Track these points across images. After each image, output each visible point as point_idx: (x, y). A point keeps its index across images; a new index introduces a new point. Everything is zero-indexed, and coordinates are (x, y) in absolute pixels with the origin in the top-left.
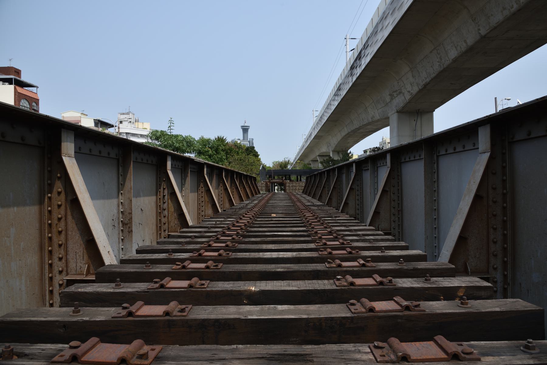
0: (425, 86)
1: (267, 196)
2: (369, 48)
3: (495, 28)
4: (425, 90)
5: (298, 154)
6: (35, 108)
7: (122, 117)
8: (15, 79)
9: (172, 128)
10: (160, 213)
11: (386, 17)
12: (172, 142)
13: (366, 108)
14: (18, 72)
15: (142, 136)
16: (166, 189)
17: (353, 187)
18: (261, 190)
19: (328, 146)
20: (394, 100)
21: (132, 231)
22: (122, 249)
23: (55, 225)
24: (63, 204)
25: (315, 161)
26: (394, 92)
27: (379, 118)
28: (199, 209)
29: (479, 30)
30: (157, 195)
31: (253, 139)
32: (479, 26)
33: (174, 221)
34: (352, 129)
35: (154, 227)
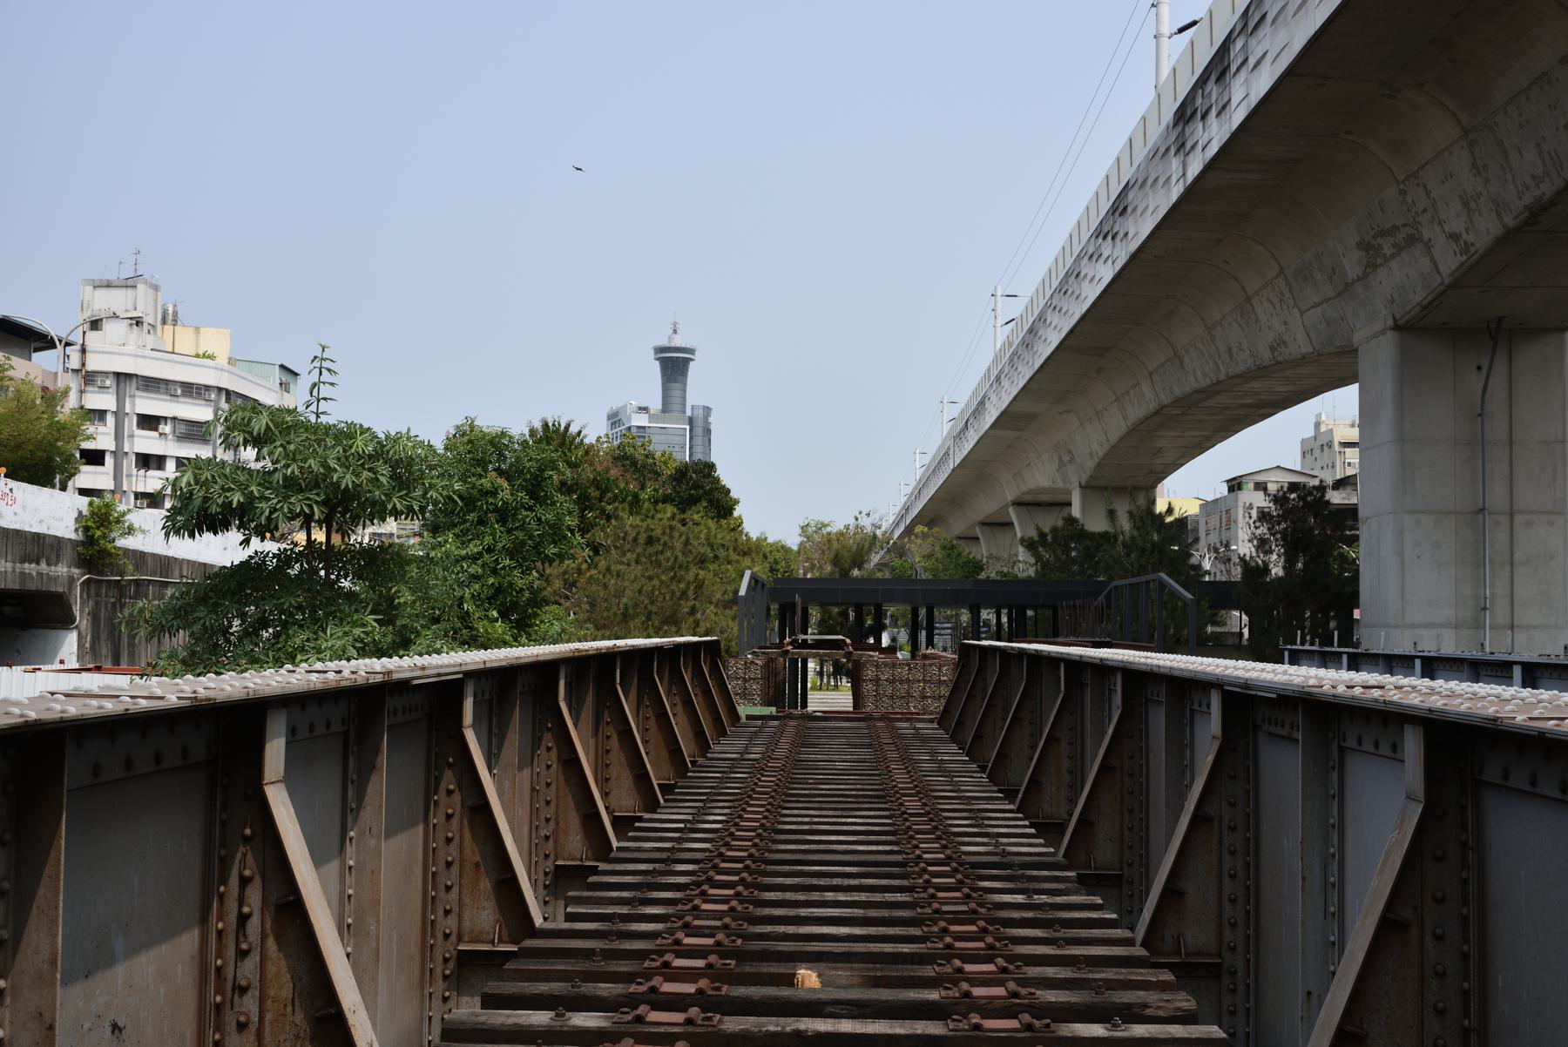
0: (1536, 214)
2: (1266, 29)
5: (919, 492)
9: (325, 391)
10: (218, 1007)
13: (1248, 300)
15: (192, 390)
16: (257, 881)
18: (746, 696)
19: (1062, 464)
20: (1382, 272)
26: (1382, 233)
27: (1306, 348)
28: (428, 903)
30: (204, 919)
31: (707, 410)
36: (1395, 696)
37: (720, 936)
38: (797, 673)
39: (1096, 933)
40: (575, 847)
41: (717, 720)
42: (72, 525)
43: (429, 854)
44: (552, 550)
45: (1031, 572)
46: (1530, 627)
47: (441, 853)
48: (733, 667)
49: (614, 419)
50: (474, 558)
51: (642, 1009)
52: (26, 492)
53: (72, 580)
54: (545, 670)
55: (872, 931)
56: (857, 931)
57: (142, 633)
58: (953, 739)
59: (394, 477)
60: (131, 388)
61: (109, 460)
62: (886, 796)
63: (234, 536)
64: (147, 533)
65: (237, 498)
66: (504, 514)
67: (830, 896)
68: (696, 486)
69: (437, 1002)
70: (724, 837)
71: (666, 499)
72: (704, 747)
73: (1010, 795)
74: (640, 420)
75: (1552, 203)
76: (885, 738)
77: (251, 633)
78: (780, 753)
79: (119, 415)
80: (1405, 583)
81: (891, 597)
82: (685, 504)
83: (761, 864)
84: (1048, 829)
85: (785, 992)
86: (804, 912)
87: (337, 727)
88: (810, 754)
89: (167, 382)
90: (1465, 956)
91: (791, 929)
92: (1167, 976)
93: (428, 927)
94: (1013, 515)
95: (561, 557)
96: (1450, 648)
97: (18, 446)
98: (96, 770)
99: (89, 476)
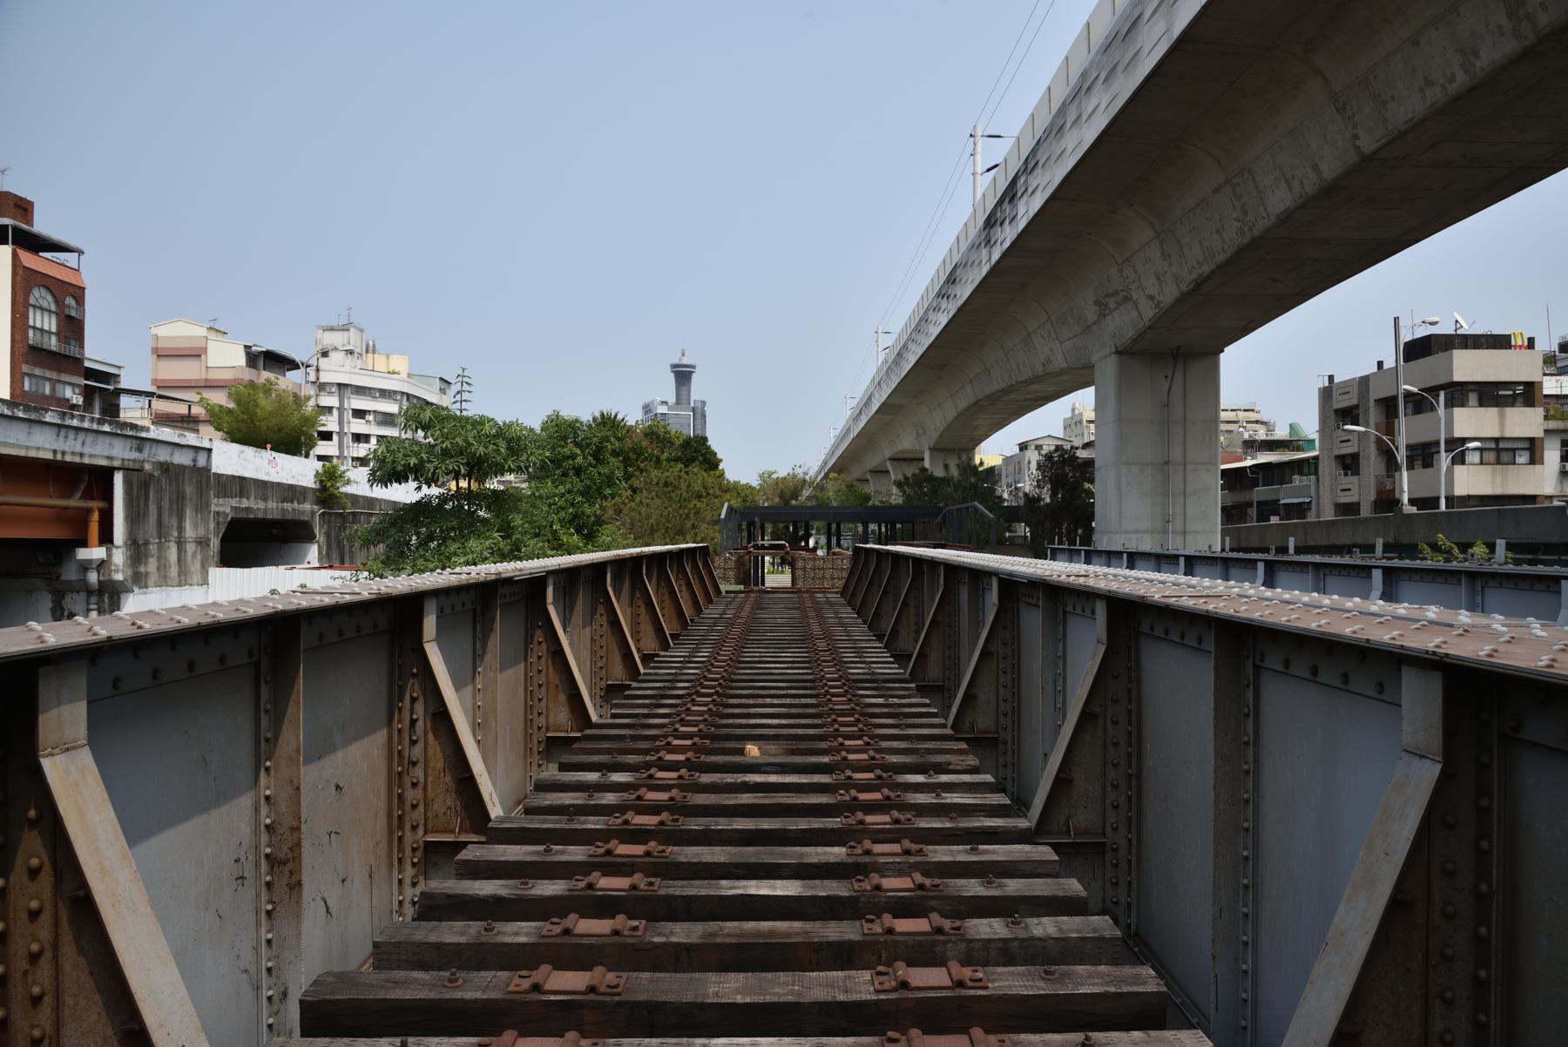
0: (1199, 284)
1: (1500, 451)
2: (1038, 170)
3: (1402, 135)
4: (1199, 295)
5: (832, 452)
6: (73, 313)
7: (330, 339)
8: (15, 229)
9: (465, 396)
11: (1089, 89)
12: (466, 441)
14: (24, 208)
15: (385, 394)
16: (421, 700)
17: (992, 648)
18: (725, 578)
19: (918, 435)
20: (1108, 318)
21: (299, 884)
22: (269, 942)
23: (18, 975)
24: (48, 906)
25: (881, 472)
26: (1108, 295)
28: (528, 708)
29: (1356, 137)
30: (390, 723)
32: (1355, 126)
33: (445, 801)
34: (987, 392)
35: (381, 824)
36: (1091, 582)
37: (701, 726)
38: (758, 564)
39: (924, 720)
40: (618, 673)
41: (707, 594)
42: (313, 479)
43: (528, 680)
44: (608, 491)
45: (900, 501)
46: (1196, 532)
47: (535, 679)
48: (718, 561)
49: (647, 409)
50: (562, 495)
51: (653, 771)
52: (283, 459)
53: (313, 513)
54: (598, 568)
55: (792, 721)
56: (783, 722)
57: (357, 545)
58: (849, 604)
59: (509, 448)
60: (348, 393)
61: (335, 437)
62: (806, 639)
63: (412, 484)
64: (358, 483)
65: (413, 461)
66: (578, 471)
67: (768, 701)
68: (696, 451)
69: (535, 767)
70: (707, 666)
71: (677, 459)
72: (698, 610)
73: (880, 638)
74: (662, 410)
75: (1208, 278)
76: (808, 604)
77: (423, 544)
78: (744, 613)
79: (341, 409)
80: (1121, 510)
81: (815, 517)
82: (688, 462)
83: (728, 681)
84: (901, 658)
85: (738, 759)
86: (752, 711)
87: (469, 606)
88: (762, 615)
89: (370, 389)
90: (1130, 733)
91: (744, 721)
92: (963, 746)
93: (528, 723)
94: (889, 466)
95: (613, 496)
96: (1147, 545)
97: (280, 430)
98: (321, 637)
99: (323, 448)
